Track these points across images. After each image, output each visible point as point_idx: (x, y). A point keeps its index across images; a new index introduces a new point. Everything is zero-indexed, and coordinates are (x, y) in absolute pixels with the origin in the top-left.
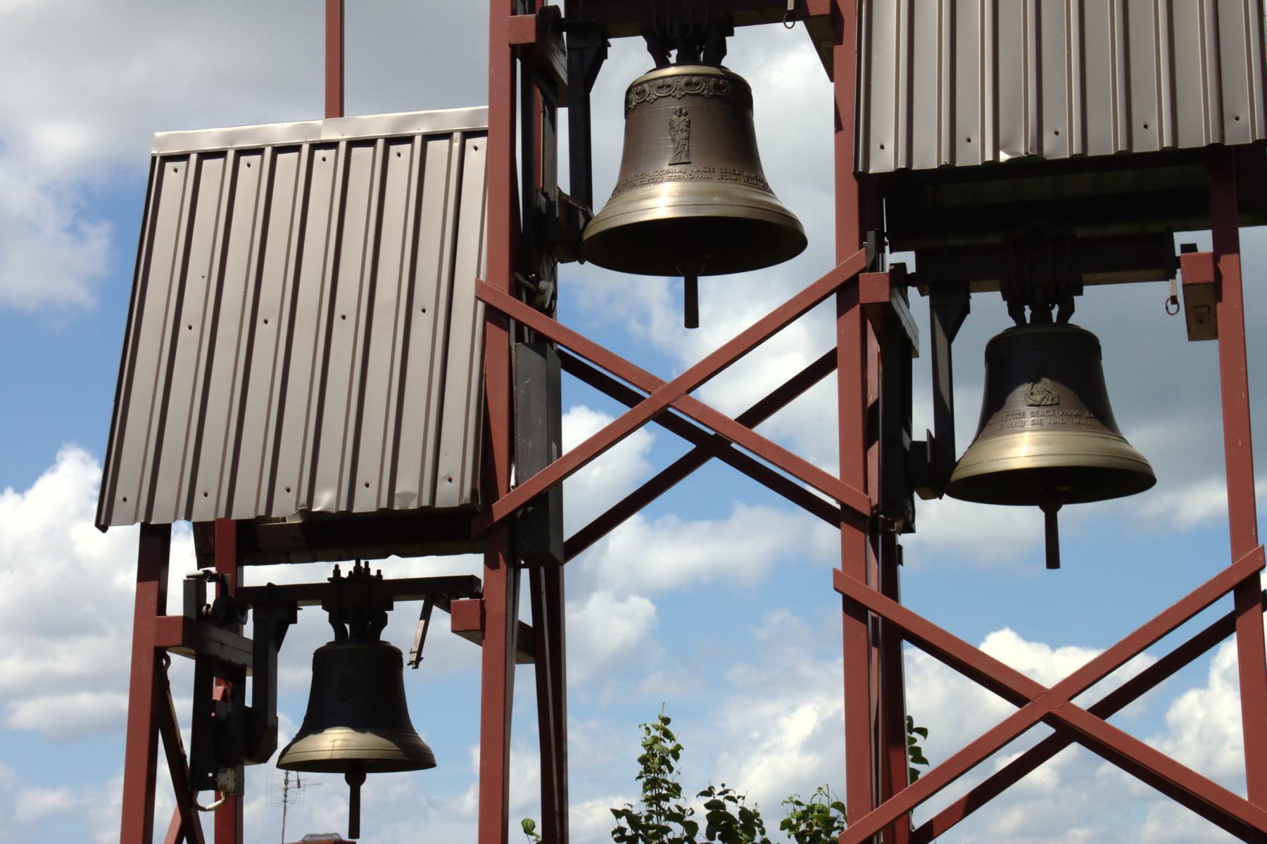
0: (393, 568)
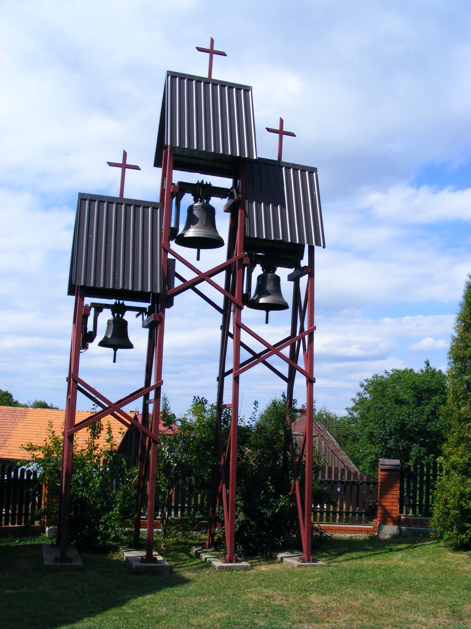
0: (127, 303)
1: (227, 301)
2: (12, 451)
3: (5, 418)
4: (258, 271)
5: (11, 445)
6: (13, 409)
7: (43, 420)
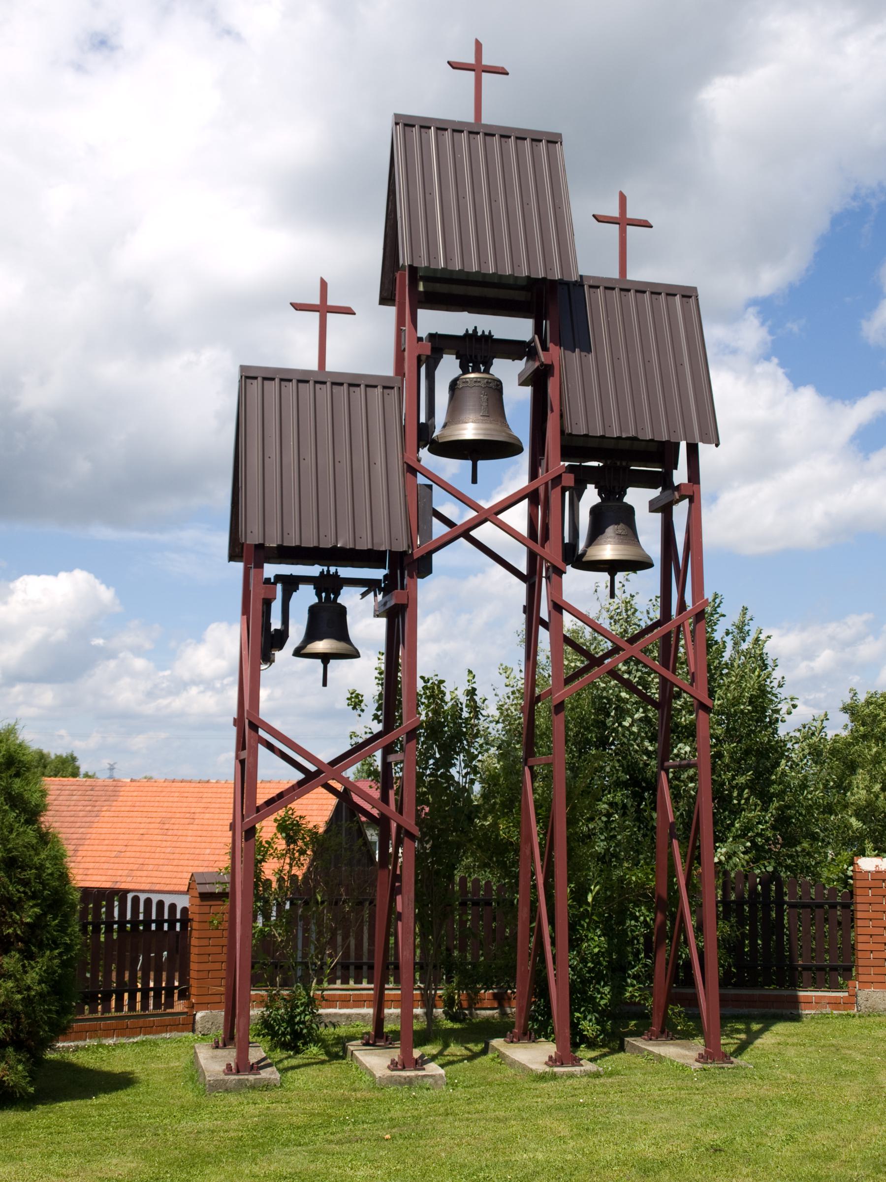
0: (345, 572)
1: (532, 558)
2: (90, 872)
3: (73, 803)
4: (591, 496)
5: (88, 859)
6: (87, 783)
7: (152, 804)
